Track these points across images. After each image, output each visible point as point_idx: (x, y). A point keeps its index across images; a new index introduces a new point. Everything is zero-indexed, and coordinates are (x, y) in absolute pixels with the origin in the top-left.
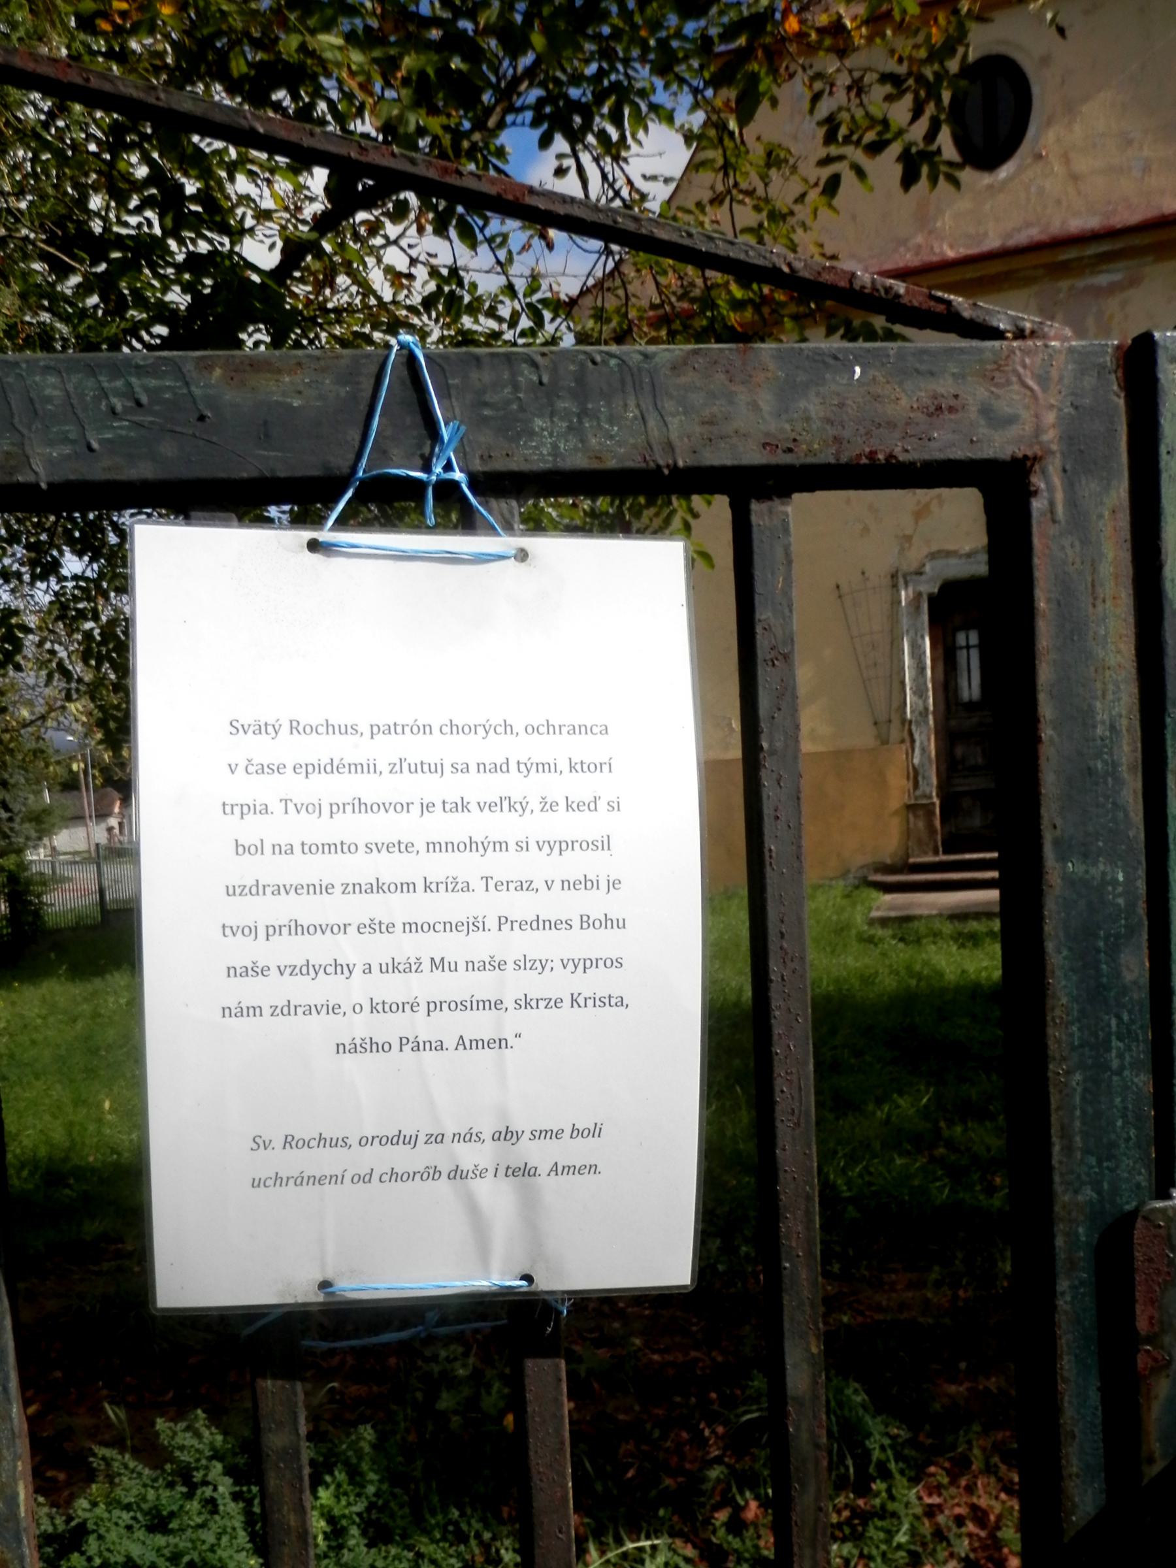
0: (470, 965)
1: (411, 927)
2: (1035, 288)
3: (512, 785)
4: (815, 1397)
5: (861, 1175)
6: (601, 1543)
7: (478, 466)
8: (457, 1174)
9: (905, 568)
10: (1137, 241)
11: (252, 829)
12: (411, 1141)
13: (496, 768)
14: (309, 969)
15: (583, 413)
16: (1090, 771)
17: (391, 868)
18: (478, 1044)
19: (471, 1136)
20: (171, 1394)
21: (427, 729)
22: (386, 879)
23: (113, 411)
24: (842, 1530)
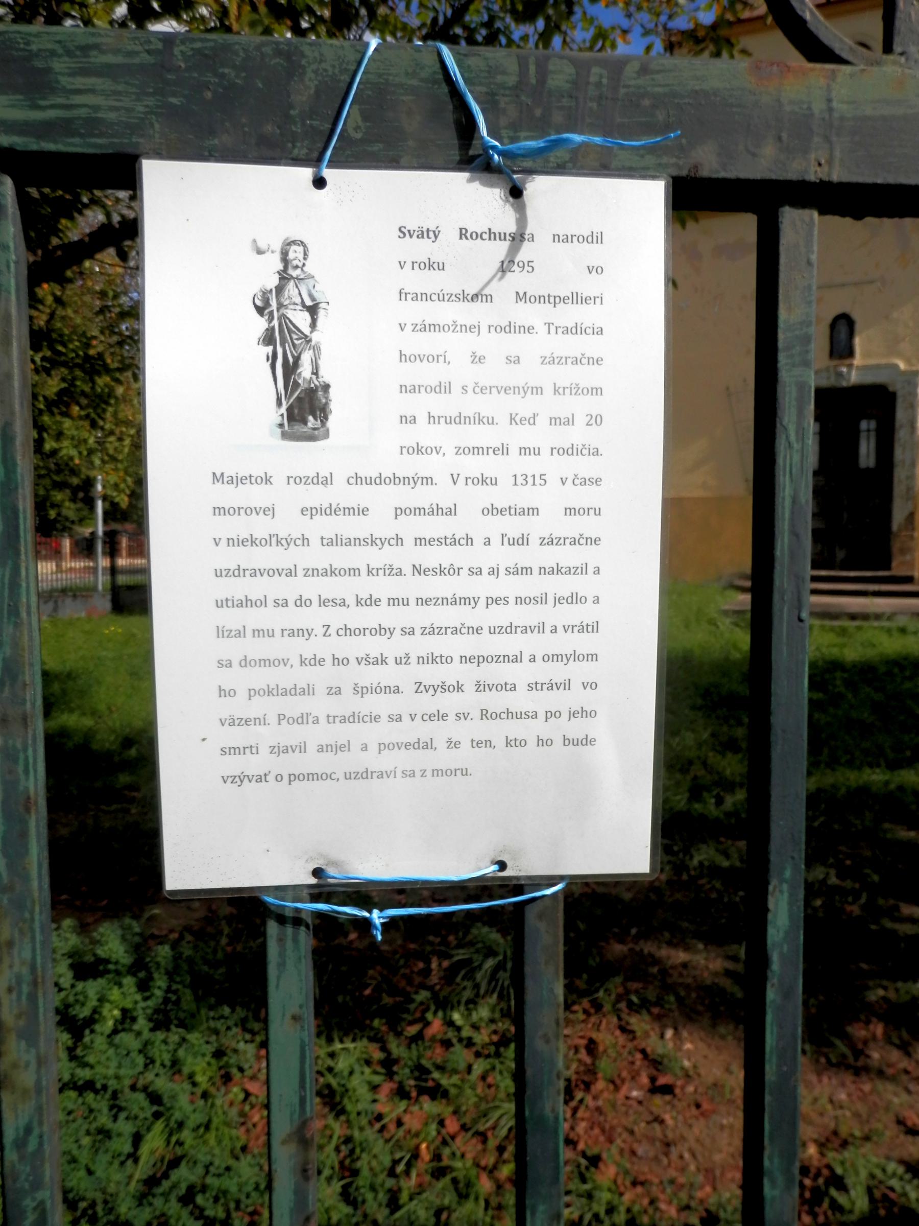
1: (422, 602)
20: (105, 902)
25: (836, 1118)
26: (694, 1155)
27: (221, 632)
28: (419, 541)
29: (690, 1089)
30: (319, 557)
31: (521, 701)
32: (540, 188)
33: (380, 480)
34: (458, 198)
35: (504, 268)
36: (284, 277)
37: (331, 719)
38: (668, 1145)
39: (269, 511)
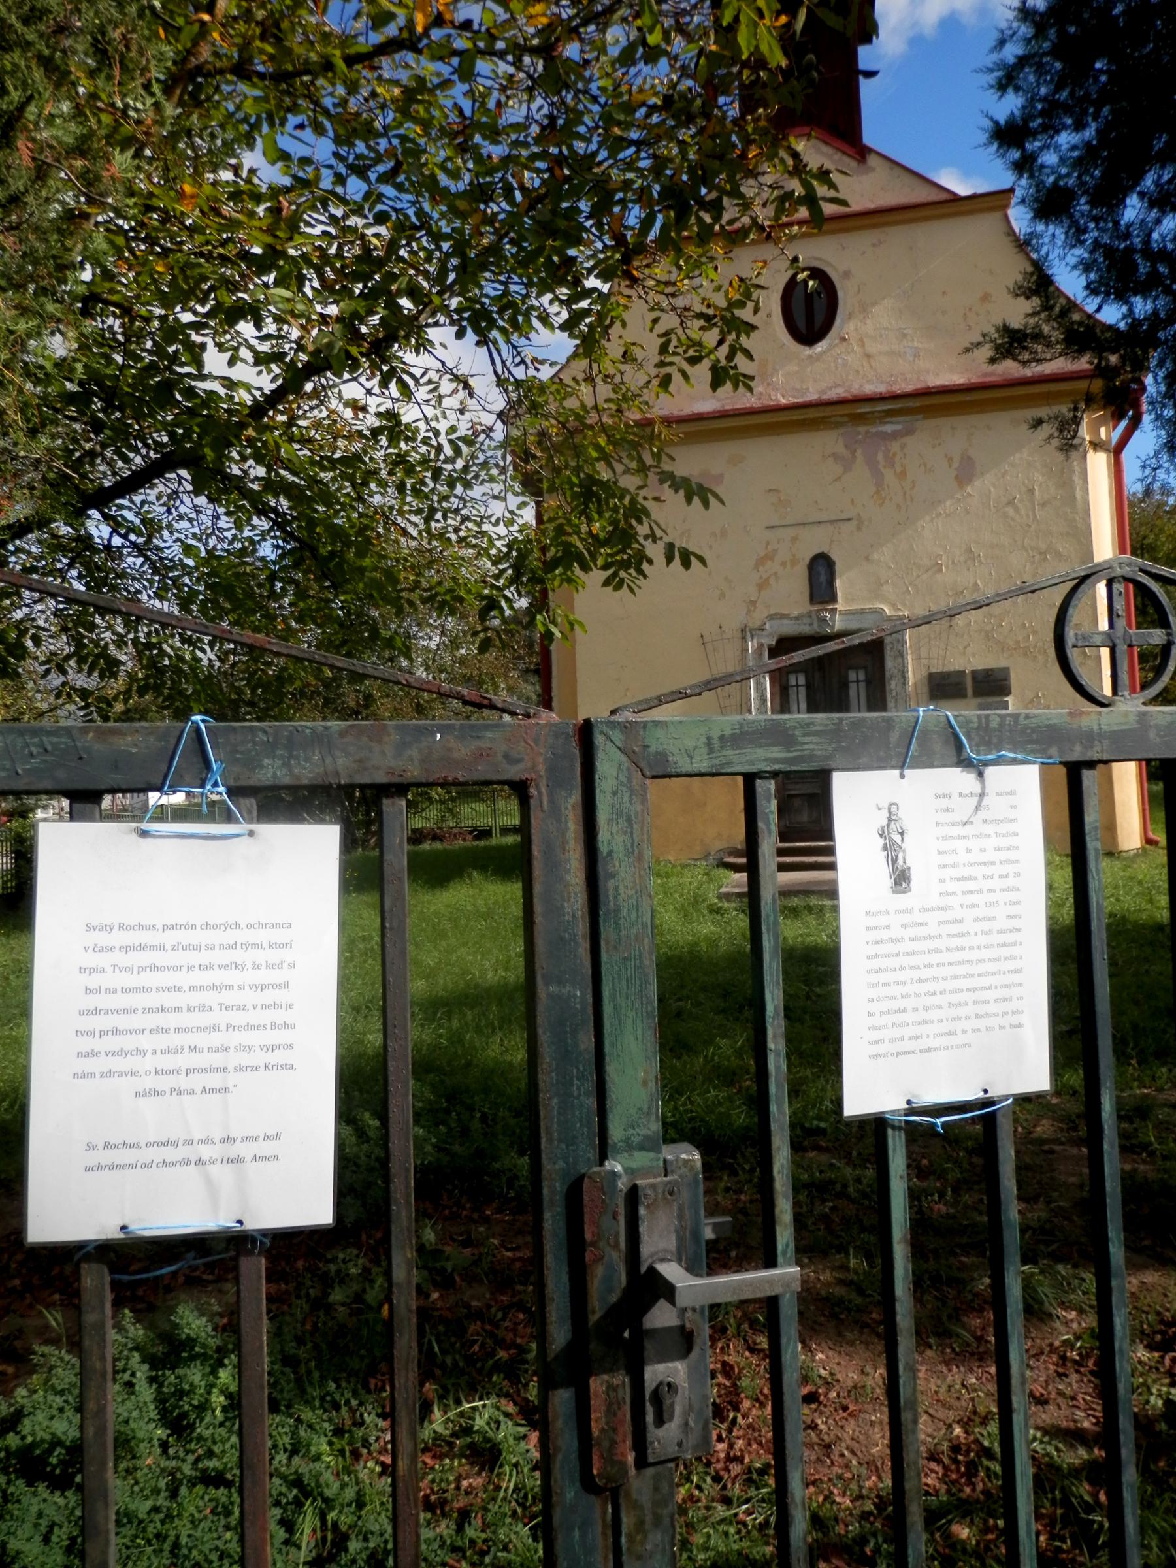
0: (210, 1049)
1: (178, 1030)
2: (841, 430)
3: (238, 956)
4: (409, 1282)
5: (684, 1104)
6: (446, 1406)
7: (232, 783)
8: (200, 1162)
9: (751, 625)
10: (911, 403)
11: (94, 981)
12: (175, 1144)
13: (229, 947)
14: (122, 1053)
15: (291, 757)
16: (562, 939)
17: (169, 999)
18: (212, 1090)
19: (208, 1141)
21: (193, 927)
22: (166, 1005)
23: (31, 755)
24: (455, 1363)
25: (972, 1399)
26: (853, 1452)
27: (869, 985)
28: (949, 936)
29: (833, 1394)
30: (908, 946)
31: (992, 1008)
32: (990, 771)
33: (932, 909)
34: (958, 779)
35: (977, 808)
36: (890, 820)
37: (914, 1023)
38: (828, 1447)
39: (888, 927)
